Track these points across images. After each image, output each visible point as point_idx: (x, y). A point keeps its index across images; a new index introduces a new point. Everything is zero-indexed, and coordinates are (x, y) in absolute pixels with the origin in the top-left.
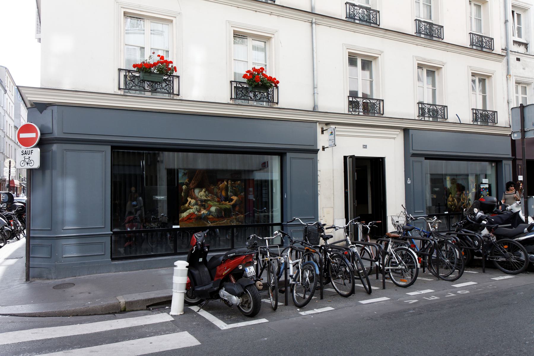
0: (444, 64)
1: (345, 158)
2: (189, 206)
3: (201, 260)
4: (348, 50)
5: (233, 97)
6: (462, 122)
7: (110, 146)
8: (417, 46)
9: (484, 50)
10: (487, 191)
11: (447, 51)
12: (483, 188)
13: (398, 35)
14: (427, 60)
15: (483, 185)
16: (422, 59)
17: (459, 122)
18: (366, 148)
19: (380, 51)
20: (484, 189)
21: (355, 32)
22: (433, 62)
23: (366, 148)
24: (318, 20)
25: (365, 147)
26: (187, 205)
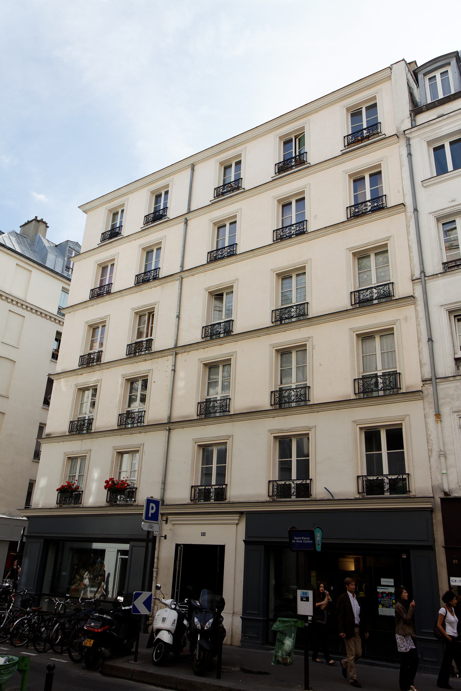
0: (311, 428)
1: (177, 545)
2: (76, 581)
3: (332, 588)
4: (358, 425)
5: (108, 501)
6: (336, 498)
7: (43, 540)
8: (274, 418)
9: (143, 415)
10: (393, 598)
11: (318, 412)
12: (383, 593)
13: (246, 415)
14: (287, 430)
15: (381, 589)
16: (278, 431)
17: (331, 498)
18: (205, 536)
19: (227, 436)
20: (385, 595)
21: (205, 425)
22: (293, 430)
23: (205, 536)
24: (171, 426)
25: (203, 534)
26: (75, 580)
